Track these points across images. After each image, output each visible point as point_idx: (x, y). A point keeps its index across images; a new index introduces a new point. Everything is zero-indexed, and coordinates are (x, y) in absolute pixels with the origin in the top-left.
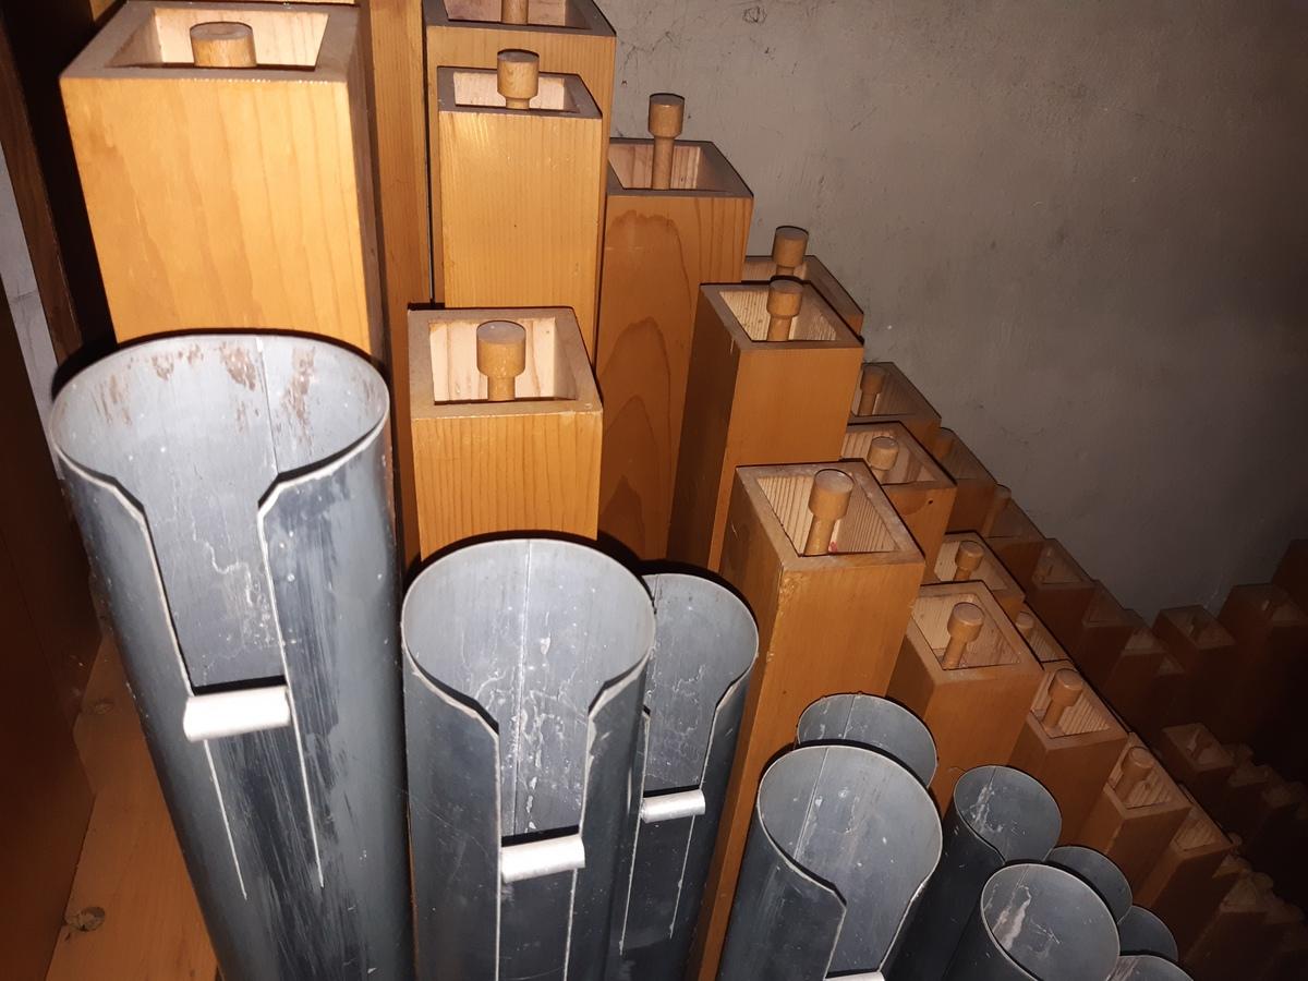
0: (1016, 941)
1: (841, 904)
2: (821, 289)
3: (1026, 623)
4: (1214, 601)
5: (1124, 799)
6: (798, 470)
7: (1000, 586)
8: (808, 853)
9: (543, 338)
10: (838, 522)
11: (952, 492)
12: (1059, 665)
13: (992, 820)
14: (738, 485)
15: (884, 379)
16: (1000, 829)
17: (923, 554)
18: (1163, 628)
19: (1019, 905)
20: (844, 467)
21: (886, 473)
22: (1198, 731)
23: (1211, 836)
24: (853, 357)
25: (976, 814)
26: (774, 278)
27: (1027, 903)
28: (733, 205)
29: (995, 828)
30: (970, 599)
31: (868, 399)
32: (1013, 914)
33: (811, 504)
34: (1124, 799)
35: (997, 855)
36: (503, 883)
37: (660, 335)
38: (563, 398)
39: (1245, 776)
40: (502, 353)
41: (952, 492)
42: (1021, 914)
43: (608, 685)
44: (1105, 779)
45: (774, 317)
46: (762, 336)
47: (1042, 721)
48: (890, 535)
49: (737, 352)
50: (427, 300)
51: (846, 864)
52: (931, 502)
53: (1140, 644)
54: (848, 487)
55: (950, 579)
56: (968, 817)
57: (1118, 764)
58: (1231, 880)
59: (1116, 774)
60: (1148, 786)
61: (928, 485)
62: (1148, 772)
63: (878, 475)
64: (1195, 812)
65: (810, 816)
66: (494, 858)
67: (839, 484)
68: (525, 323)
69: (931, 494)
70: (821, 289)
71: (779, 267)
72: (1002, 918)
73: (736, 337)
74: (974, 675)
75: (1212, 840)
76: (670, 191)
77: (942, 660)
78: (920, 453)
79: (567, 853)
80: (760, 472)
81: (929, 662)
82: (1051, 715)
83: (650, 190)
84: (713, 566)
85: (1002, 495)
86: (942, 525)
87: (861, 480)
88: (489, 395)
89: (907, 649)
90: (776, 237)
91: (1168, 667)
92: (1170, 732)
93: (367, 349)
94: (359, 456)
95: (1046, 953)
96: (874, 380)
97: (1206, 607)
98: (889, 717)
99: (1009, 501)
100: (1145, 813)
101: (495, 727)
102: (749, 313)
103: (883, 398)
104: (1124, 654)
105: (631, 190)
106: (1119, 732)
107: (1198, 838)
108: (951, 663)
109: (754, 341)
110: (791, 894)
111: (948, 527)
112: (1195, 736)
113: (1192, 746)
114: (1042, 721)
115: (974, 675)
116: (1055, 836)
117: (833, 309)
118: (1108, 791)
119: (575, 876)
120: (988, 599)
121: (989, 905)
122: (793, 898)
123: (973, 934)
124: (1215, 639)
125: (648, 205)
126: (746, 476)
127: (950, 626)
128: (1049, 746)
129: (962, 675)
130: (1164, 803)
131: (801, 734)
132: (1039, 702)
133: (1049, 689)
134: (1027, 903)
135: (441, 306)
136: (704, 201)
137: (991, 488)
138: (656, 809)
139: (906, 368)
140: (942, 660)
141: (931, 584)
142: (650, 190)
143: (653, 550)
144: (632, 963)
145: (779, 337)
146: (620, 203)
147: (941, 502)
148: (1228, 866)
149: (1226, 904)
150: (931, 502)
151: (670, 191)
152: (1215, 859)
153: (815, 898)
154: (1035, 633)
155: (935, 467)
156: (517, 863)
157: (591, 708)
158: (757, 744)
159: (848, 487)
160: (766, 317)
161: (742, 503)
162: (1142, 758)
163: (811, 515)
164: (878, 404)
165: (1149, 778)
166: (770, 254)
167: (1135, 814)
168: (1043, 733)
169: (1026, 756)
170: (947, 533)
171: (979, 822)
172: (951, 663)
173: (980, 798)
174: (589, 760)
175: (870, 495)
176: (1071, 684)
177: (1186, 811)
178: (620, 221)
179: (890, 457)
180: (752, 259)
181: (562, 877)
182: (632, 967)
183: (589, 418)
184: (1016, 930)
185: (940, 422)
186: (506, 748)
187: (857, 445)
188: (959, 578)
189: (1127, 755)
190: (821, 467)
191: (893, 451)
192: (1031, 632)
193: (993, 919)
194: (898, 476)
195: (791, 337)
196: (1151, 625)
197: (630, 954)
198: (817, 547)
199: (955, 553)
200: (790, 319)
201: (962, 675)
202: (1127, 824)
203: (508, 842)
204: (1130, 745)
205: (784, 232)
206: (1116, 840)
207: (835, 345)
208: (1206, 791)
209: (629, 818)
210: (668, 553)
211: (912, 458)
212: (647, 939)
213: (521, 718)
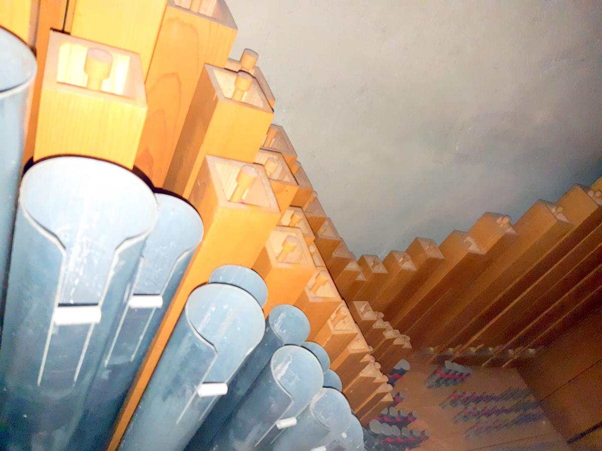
0: (282, 378)
1: (215, 352)
2: (258, 80)
3: (313, 249)
4: (383, 255)
5: (334, 326)
6: (234, 162)
7: (306, 232)
8: (204, 331)
9: (122, 63)
10: (247, 191)
11: (296, 188)
12: (322, 268)
13: (282, 328)
14: (205, 164)
15: (277, 133)
16: (284, 331)
17: (280, 210)
18: (362, 262)
19: (286, 362)
20: (256, 166)
21: (271, 174)
22: (366, 305)
23: (363, 346)
24: (267, 119)
25: (276, 323)
26: (240, 71)
27: (290, 362)
28: (227, 30)
29: (283, 330)
30: (294, 235)
31: (269, 140)
32: (284, 365)
33: (238, 179)
34: (334, 326)
35: (281, 342)
36: (55, 326)
37: (180, 83)
38: (128, 97)
39: (379, 324)
40: (99, 67)
41: (296, 188)
42: (287, 367)
43: (128, 239)
44: (329, 317)
45: (237, 89)
46: (229, 95)
47: (310, 289)
48: (268, 200)
49: (217, 100)
50: (60, 28)
51: (219, 337)
52: (287, 191)
53: (352, 266)
54: (255, 175)
55: (287, 225)
56: (273, 325)
57: (335, 311)
58: (367, 363)
59: (333, 316)
60: (344, 322)
61: (288, 183)
62: (345, 317)
63: (268, 174)
64: (360, 335)
65: (208, 314)
66: (51, 312)
67: (252, 172)
68: (114, 55)
69: (288, 188)
70: (258, 80)
71: (242, 67)
72: (278, 367)
73: (217, 93)
74: (290, 266)
75: (363, 347)
76: (199, 14)
77: (277, 258)
78: (287, 168)
79: (92, 316)
80: (216, 159)
81: (272, 257)
82: (314, 288)
83: (188, 10)
84: (185, 196)
85: (315, 195)
86: (289, 202)
87: (261, 174)
88: (87, 85)
89: (264, 252)
90: (270, 128)
91: (361, 277)
92: (356, 303)
93: (26, 39)
94: (13, 96)
95: (293, 384)
96: (273, 132)
97: (379, 256)
98: (251, 278)
99: (316, 198)
100: (341, 333)
101: (64, 247)
102: (225, 84)
103: (275, 142)
104: (345, 269)
105: (179, 7)
106: (339, 298)
107: (359, 345)
108: (280, 259)
109: (225, 98)
110: (194, 347)
111: (293, 202)
112: (364, 307)
113: (362, 309)
114: (310, 289)
115: (290, 266)
116: (306, 337)
117: (264, 93)
118: (329, 322)
119: (90, 334)
120: (301, 236)
121: (275, 361)
122: (194, 349)
123: (265, 371)
124: (381, 269)
125: (186, 17)
126: (210, 160)
127: (284, 244)
128: (311, 300)
129: (284, 266)
130: (348, 330)
131: (211, 279)
132: (312, 282)
133: (317, 277)
134: (290, 362)
135: (68, 34)
136: (215, 24)
137: (310, 191)
138: (136, 303)
139: (288, 131)
140: (277, 258)
141: (280, 225)
142: (188, 10)
143: (157, 184)
144: (110, 371)
145: (237, 98)
146: (173, 12)
147: (291, 191)
148: (368, 358)
149: (362, 373)
150: (287, 191)
151: (199, 14)
152: (362, 355)
153: (204, 348)
154: (315, 254)
155: (292, 176)
156: (61, 317)
157: (117, 248)
158: (188, 284)
159: (255, 175)
160: (233, 88)
161: (205, 171)
162: (344, 310)
163: (236, 184)
164: (273, 143)
165: (345, 319)
166: (239, 60)
167: (337, 333)
168: (310, 295)
169: (301, 303)
170: (291, 206)
171: (277, 328)
172: (280, 259)
173: (280, 318)
174: (112, 273)
175: (264, 181)
176: (325, 276)
177: (357, 334)
178: (171, 20)
179: (275, 167)
180: (230, 60)
181: (86, 327)
182: (110, 373)
183: (139, 112)
184: (283, 372)
185: (297, 158)
186: (68, 259)
187: (262, 158)
188: (290, 225)
189: (339, 309)
190: (245, 164)
191: (276, 165)
192: (314, 253)
193: (275, 367)
194: (276, 176)
195: (243, 100)
196: (358, 259)
197: (109, 367)
198: (236, 199)
199: (291, 214)
200: (243, 91)
201: (284, 266)
202: (333, 336)
203: (61, 305)
204: (341, 305)
205: (247, 51)
206: (328, 342)
207: (263, 110)
208: (366, 328)
209: (122, 306)
210: (164, 185)
211: (283, 170)
212: (120, 360)
213: (75, 250)
